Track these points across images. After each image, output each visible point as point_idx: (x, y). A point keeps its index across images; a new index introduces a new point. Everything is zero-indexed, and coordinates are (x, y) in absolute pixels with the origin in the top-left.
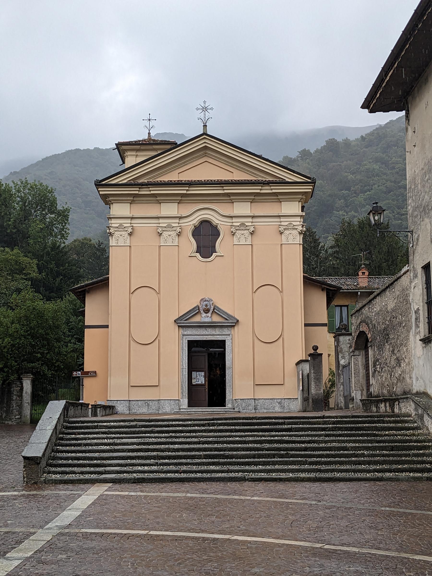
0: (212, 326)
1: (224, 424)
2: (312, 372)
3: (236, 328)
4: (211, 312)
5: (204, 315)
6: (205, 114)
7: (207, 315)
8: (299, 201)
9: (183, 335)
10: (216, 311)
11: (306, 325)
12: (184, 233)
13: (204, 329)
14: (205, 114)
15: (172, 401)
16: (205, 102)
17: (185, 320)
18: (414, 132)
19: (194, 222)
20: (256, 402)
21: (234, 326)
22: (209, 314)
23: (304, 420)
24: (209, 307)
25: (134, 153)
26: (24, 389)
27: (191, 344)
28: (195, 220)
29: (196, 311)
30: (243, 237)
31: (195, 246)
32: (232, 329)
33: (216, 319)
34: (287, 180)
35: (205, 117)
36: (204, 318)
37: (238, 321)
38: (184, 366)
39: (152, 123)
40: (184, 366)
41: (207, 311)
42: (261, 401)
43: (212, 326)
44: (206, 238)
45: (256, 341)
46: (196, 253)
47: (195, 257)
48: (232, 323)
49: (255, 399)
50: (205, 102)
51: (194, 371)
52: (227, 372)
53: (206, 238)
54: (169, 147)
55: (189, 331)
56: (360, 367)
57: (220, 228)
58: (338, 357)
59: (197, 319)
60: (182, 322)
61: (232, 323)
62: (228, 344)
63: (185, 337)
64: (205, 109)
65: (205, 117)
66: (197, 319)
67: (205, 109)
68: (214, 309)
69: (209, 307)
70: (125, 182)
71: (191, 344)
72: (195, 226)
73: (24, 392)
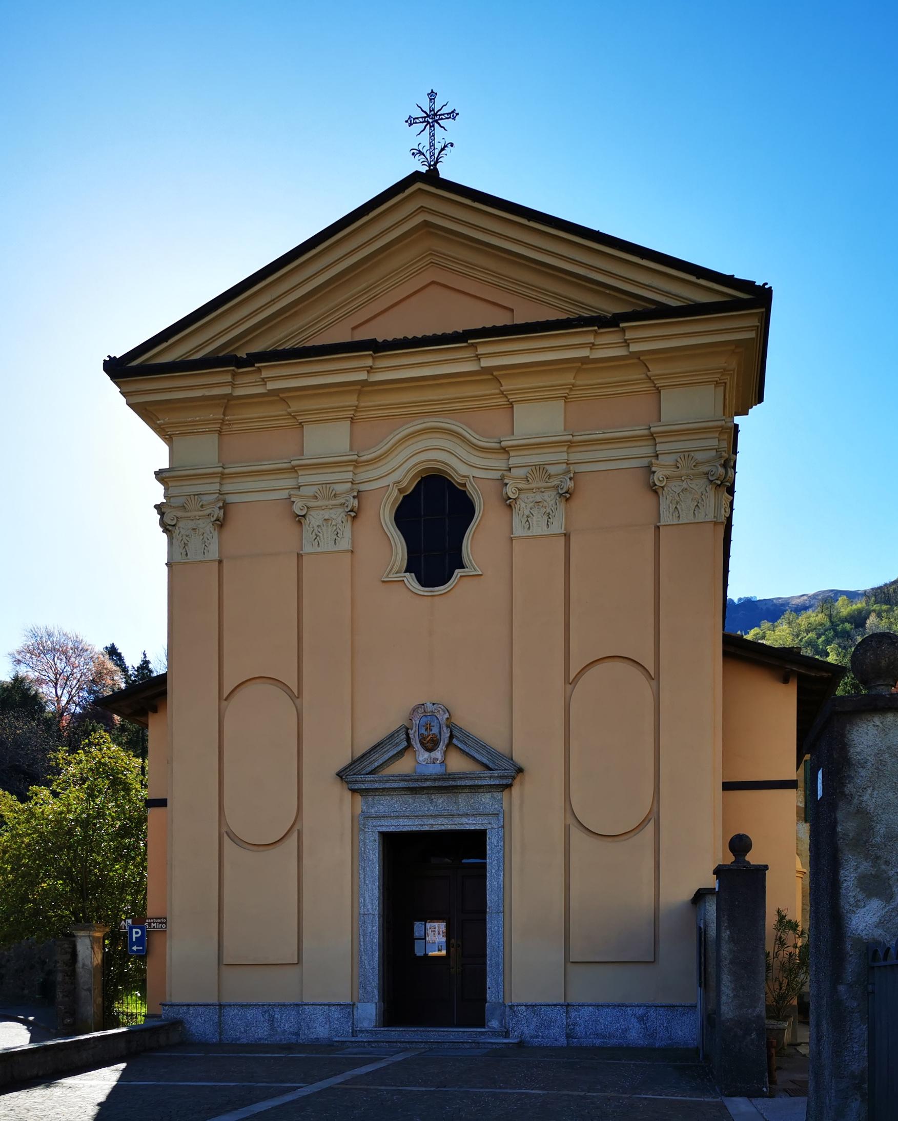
0: (447, 786)
2: (726, 934)
3: (515, 790)
4: (442, 746)
5: (423, 756)
6: (432, 136)
7: (433, 755)
8: (717, 384)
9: (367, 817)
10: (456, 738)
11: (728, 786)
12: (368, 515)
13: (424, 798)
14: (432, 136)
15: (333, 1009)
16: (432, 95)
17: (370, 773)
19: (396, 476)
20: (573, 1014)
21: (509, 786)
22: (438, 754)
24: (435, 730)
26: (80, 957)
27: (396, 847)
28: (395, 474)
29: (401, 741)
30: (538, 521)
31: (400, 556)
32: (507, 791)
33: (457, 764)
35: (432, 145)
36: (420, 762)
38: (370, 907)
40: (370, 907)
41: (430, 745)
42: (586, 1011)
43: (447, 786)
44: (435, 524)
46: (406, 572)
47: (401, 583)
48: (504, 774)
49: (568, 1005)
50: (432, 95)
51: (448, 927)
52: (488, 926)
53: (435, 524)
55: (383, 804)
57: (472, 491)
58: (835, 885)
59: (404, 766)
60: (358, 776)
61: (504, 774)
62: (492, 841)
63: (371, 823)
64: (432, 119)
65: (432, 145)
66: (404, 766)
68: (451, 737)
69: (435, 730)
71: (396, 847)
72: (400, 491)
73: (80, 964)
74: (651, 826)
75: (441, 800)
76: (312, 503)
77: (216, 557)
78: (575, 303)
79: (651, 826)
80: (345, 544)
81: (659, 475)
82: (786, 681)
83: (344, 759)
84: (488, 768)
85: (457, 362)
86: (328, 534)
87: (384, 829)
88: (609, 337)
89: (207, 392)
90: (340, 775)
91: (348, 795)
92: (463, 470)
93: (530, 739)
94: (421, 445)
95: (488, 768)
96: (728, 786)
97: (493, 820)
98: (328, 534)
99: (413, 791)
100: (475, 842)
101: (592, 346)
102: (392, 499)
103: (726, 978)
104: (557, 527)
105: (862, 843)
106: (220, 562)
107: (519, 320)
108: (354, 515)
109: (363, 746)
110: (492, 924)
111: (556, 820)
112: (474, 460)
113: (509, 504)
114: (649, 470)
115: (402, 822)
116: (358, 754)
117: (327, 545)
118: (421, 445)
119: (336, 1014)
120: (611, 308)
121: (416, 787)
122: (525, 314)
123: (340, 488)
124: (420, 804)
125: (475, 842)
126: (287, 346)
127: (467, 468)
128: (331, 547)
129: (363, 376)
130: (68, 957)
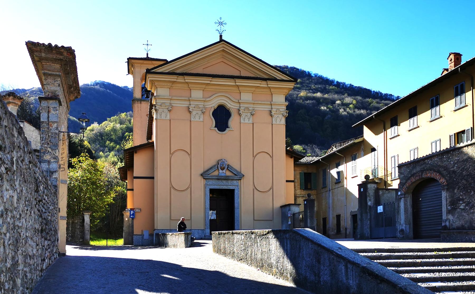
0: (227, 179)
1: (411, 257)
3: (242, 180)
5: (221, 171)
10: (229, 168)
13: (220, 181)
16: (221, 18)
18: (141, 117)
19: (213, 105)
22: (224, 171)
23: (462, 252)
25: (140, 65)
26: (85, 221)
28: (214, 103)
33: (228, 174)
34: (278, 78)
37: (244, 176)
39: (149, 47)
44: (222, 117)
45: (255, 190)
48: (239, 176)
50: (221, 18)
53: (222, 117)
54: (162, 63)
55: (210, 182)
56: (409, 206)
59: (216, 173)
60: (204, 175)
62: (236, 192)
63: (208, 186)
67: (221, 24)
70: (167, 71)
71: (212, 191)
73: (85, 223)
74: (271, 190)
75: (224, 182)
76: (194, 109)
77: (169, 119)
78: (259, 75)
79: (271, 190)
80: (201, 120)
81: (273, 113)
82: (291, 158)
83: (202, 171)
84: (236, 175)
85: (230, 82)
86: (197, 117)
87: (213, 187)
88: (264, 82)
89: (170, 80)
90: (201, 175)
91: (203, 179)
92: (229, 105)
93: (246, 170)
94: (220, 99)
95: (236, 175)
96: (287, 181)
97: (237, 187)
98: (197, 117)
99: (218, 179)
100: (233, 191)
101: (260, 84)
102: (213, 110)
103: (308, 219)
104: (251, 121)
105: (369, 196)
106: (170, 120)
107: (243, 75)
108: (203, 113)
109: (206, 169)
110: (236, 211)
111: (251, 187)
112: (232, 104)
113: (240, 115)
114: (271, 112)
115: (215, 186)
116: (205, 170)
117: (197, 119)
118: (220, 99)
119: (200, 232)
120: (266, 77)
121: (219, 178)
122: (244, 74)
123: (200, 106)
124: (220, 182)
125: (233, 191)
126: (190, 72)
127: (231, 106)
128: (198, 120)
129: (209, 82)
130: (81, 221)
